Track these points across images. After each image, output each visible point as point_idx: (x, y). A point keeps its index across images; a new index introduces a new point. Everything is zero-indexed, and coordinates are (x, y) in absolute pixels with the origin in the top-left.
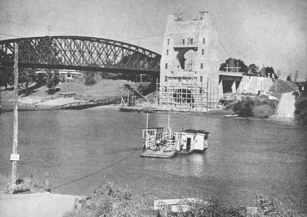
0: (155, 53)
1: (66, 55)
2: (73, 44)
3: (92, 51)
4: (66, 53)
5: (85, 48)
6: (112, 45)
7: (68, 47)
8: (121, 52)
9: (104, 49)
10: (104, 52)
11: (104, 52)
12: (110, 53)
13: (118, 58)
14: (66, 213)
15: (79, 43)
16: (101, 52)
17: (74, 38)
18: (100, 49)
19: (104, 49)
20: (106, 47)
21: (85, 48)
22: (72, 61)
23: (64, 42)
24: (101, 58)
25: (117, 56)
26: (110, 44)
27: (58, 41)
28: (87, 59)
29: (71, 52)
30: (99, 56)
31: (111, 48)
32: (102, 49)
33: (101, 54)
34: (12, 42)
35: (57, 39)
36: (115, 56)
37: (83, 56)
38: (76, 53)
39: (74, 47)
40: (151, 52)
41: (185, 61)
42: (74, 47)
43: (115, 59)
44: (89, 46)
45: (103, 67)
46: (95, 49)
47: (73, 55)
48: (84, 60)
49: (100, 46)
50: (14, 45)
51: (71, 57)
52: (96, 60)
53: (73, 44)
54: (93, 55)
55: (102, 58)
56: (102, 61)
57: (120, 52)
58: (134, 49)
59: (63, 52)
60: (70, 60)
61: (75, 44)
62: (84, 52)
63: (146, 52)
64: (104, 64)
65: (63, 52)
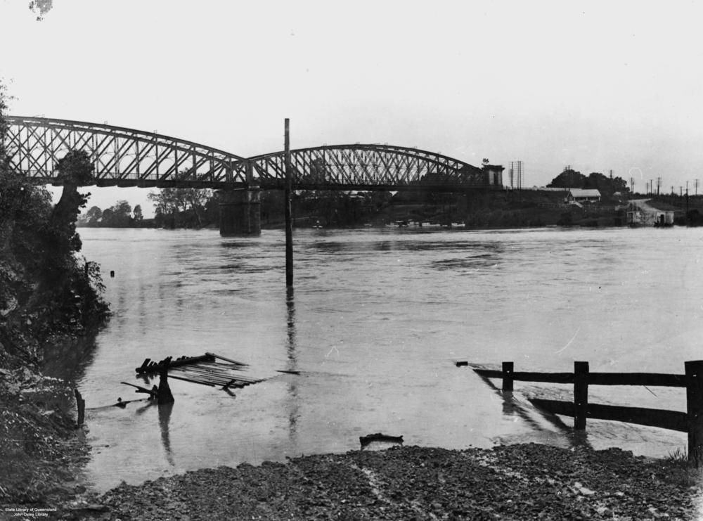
0: (461, 163)
1: (344, 171)
2: (352, 154)
3: (366, 163)
4: (332, 167)
5: (368, 160)
6: (393, 152)
7: (346, 160)
8: (417, 163)
9: (393, 161)
10: (393, 164)
11: (393, 164)
12: (391, 163)
13: (401, 170)
14: (288, 315)
15: (348, 154)
16: (378, 164)
17: (342, 147)
18: (388, 160)
19: (393, 161)
20: (397, 157)
21: (368, 160)
22: (352, 178)
23: (342, 153)
24: (390, 173)
25: (401, 168)
26: (390, 152)
27: (333, 153)
28: (360, 174)
29: (338, 167)
30: (377, 170)
31: (402, 158)
32: (391, 160)
33: (390, 167)
34: (258, 160)
35: (318, 150)
36: (409, 169)
37: (365, 170)
38: (356, 168)
39: (354, 159)
40: (457, 162)
41: (503, 171)
42: (354, 159)
43: (398, 172)
44: (374, 156)
45: (370, 184)
46: (382, 160)
47: (340, 171)
48: (368, 175)
49: (389, 156)
50: (276, 160)
51: (350, 173)
52: (383, 175)
53: (352, 154)
54: (379, 169)
55: (392, 173)
56: (391, 176)
57: (415, 163)
58: (433, 158)
59: (340, 167)
60: (337, 177)
61: (356, 155)
62: (367, 166)
63: (450, 162)
64: (99, 174)
65: (340, 167)
